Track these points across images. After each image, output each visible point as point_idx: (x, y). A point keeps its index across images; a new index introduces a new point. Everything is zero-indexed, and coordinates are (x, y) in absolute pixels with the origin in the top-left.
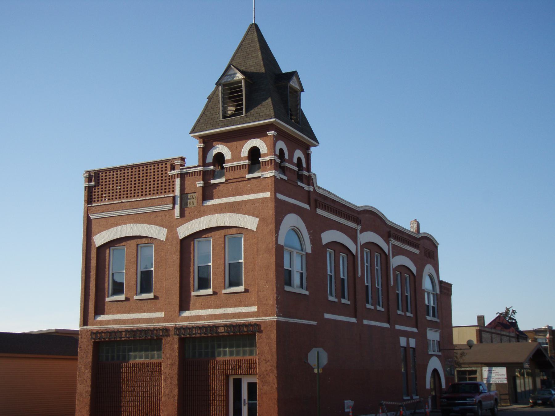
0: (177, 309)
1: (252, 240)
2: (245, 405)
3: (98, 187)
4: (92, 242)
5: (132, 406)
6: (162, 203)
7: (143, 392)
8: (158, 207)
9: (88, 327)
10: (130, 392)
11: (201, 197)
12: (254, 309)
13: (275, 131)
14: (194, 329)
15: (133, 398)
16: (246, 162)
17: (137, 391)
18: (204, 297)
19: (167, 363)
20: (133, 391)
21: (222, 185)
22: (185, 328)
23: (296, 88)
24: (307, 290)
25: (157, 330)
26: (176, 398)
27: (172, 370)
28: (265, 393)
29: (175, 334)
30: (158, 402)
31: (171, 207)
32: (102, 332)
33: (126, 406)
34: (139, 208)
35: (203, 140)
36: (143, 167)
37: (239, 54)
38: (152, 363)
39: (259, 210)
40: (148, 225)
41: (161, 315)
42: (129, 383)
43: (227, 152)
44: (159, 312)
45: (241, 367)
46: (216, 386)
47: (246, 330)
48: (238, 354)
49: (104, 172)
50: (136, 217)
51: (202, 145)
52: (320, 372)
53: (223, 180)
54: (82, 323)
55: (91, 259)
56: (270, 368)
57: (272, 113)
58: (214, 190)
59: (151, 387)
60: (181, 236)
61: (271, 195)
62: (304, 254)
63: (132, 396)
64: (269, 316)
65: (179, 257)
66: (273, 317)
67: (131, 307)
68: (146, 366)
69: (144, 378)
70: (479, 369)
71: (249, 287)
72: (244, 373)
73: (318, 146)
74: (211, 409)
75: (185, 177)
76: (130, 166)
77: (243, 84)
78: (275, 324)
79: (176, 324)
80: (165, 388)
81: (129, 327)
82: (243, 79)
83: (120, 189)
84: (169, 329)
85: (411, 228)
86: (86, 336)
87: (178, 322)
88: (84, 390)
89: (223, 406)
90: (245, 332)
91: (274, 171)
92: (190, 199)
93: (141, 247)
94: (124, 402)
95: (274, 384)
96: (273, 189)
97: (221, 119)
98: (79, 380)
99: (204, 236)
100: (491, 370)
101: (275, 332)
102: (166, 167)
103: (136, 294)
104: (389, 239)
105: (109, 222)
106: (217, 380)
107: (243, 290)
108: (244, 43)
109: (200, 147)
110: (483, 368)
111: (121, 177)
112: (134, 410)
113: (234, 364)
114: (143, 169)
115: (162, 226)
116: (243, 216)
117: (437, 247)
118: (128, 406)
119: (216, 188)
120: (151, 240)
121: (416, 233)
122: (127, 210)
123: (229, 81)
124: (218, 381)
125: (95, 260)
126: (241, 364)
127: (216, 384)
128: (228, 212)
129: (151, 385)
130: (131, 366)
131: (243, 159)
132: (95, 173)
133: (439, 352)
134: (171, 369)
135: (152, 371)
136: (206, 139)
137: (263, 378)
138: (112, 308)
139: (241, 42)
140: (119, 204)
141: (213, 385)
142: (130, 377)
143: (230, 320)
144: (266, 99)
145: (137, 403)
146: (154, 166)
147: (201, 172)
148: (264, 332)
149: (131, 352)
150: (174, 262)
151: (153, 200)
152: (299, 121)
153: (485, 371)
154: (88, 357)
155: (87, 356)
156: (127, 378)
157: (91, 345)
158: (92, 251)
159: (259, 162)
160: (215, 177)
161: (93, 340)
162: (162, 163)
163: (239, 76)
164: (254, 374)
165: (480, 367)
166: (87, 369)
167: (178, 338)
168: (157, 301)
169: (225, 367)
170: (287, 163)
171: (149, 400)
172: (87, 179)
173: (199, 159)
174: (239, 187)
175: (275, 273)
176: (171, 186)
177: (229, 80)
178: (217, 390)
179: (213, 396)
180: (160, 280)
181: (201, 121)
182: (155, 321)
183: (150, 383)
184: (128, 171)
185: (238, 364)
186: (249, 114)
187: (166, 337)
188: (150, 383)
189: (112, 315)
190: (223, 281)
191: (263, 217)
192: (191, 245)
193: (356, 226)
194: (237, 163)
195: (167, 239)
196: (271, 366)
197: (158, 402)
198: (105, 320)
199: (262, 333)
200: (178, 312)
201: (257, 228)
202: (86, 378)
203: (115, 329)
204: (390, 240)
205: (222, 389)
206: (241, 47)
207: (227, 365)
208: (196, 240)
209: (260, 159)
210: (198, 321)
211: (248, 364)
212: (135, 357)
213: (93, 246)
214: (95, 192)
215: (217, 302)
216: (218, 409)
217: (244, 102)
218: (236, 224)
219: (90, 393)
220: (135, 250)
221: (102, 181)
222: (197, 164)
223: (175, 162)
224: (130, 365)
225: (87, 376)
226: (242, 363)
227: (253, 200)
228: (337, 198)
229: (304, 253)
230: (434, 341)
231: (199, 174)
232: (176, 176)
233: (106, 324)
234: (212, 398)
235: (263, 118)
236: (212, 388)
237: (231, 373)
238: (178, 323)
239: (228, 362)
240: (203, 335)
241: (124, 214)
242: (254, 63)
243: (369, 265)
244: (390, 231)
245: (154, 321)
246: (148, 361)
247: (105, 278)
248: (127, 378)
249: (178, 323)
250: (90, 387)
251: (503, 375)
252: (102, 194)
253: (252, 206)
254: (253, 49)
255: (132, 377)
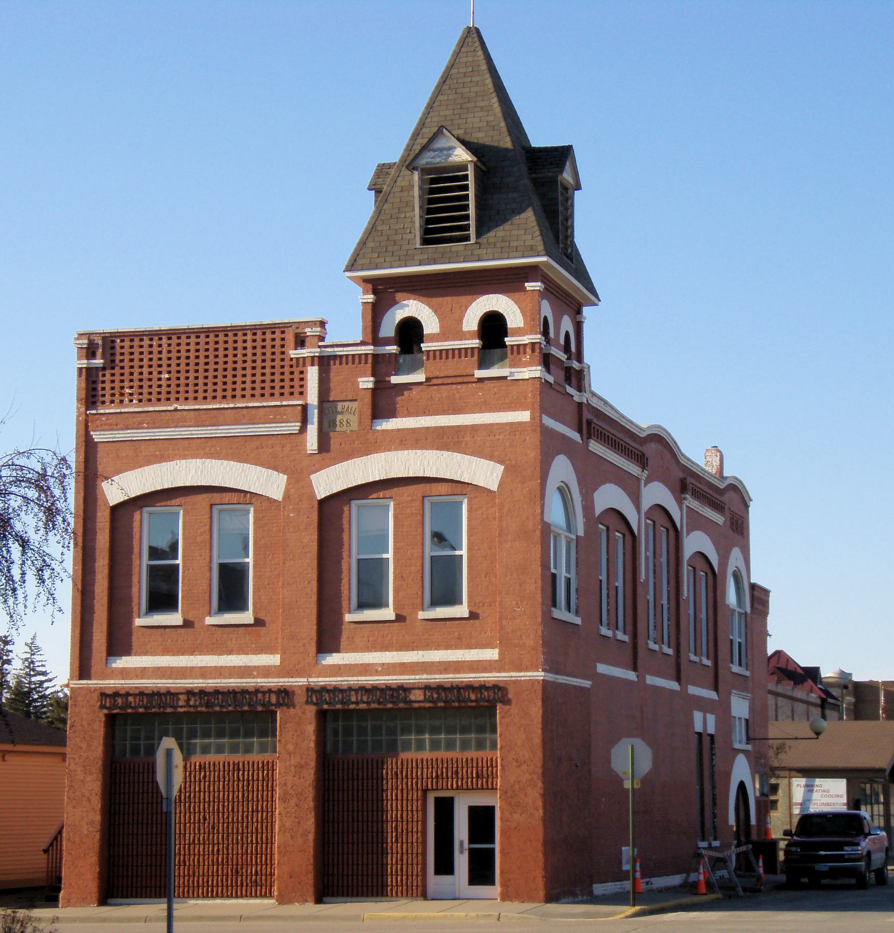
0: (313, 648)
1: (487, 510)
2: (462, 852)
3: (113, 372)
4: (98, 493)
5: (199, 855)
6: (275, 418)
7: (225, 825)
8: (266, 425)
9: (93, 683)
10: (195, 823)
11: (368, 412)
12: (492, 654)
13: (543, 282)
14: (353, 693)
15: (201, 837)
16: (476, 343)
17: (211, 821)
18: (375, 625)
19: (288, 763)
20: (202, 821)
21: (415, 391)
22: (330, 690)
23: (568, 182)
24: (577, 613)
25: (264, 693)
26: (311, 837)
27: (300, 778)
28: (515, 828)
29: (307, 703)
30: (264, 845)
31: (298, 428)
32: (128, 694)
33: (185, 855)
34: (219, 425)
35: (373, 286)
36: (226, 335)
37: (446, 97)
38: (248, 763)
39: (505, 449)
40: (239, 464)
41: (274, 660)
42: (192, 805)
43: (429, 318)
44: (266, 653)
45: (457, 772)
46: (399, 813)
47: (473, 697)
48: (450, 746)
49: (127, 339)
50: (209, 444)
51: (370, 298)
52: (635, 786)
53: (419, 377)
54: (77, 674)
55: (97, 532)
56: (527, 776)
57: (541, 247)
58: (399, 399)
59: (245, 814)
60: (321, 494)
61: (533, 418)
62: (572, 539)
63: (199, 833)
64: (527, 669)
65: (315, 537)
66: (535, 674)
67: (196, 640)
68: (234, 768)
69: (229, 794)
70: (783, 783)
71: (479, 608)
72: (465, 787)
73: (596, 305)
74: (389, 859)
75: (329, 365)
76: (194, 329)
77: (470, 173)
78: (539, 689)
79: (310, 680)
80: (284, 815)
81: (196, 685)
82: (471, 161)
83: (169, 379)
84: (293, 692)
85: (706, 465)
86: (88, 702)
87: (315, 677)
88: (83, 818)
89: (417, 853)
90: (472, 701)
91: (539, 368)
92: (342, 413)
93: (220, 511)
94: (180, 845)
95: (537, 810)
96: (537, 406)
97: (418, 246)
98: (69, 798)
99: (373, 496)
100: (812, 786)
101: (539, 703)
102: (283, 339)
103: (210, 614)
104: (683, 496)
105: (141, 452)
106: (402, 800)
107: (466, 615)
108: (454, 71)
109: (366, 301)
110: (794, 779)
111: (169, 352)
112: (204, 863)
113: (442, 768)
114: (226, 339)
115: (275, 468)
116: (467, 458)
117: (749, 506)
118: (189, 855)
119: (403, 395)
120: (245, 496)
121: (717, 476)
122: (187, 429)
123: (438, 163)
124: (405, 802)
125: (108, 534)
126: (457, 767)
127: (399, 807)
128: (432, 448)
129: (245, 809)
130: (197, 767)
131: (468, 336)
132: (104, 339)
133: (747, 744)
134: (297, 777)
135: (248, 780)
136: (380, 285)
137: (511, 797)
138: (149, 641)
139: (447, 67)
140: (168, 413)
141: (392, 811)
142: (195, 792)
143: (437, 676)
144: (520, 211)
145: (211, 849)
146: (254, 334)
147: (370, 356)
148: (514, 702)
149: (195, 737)
150: (303, 548)
151: (254, 411)
152: (570, 254)
153: (798, 785)
154: (93, 748)
155: (89, 746)
156: (187, 794)
157: (101, 721)
158: (99, 514)
159: (504, 345)
160: (399, 369)
161: (105, 711)
162: (273, 330)
163: (461, 155)
164: (492, 789)
165: (786, 777)
166: (91, 774)
167: (315, 712)
168: (262, 630)
169: (422, 774)
170: (553, 348)
171: (242, 840)
172: (85, 351)
173: (364, 328)
174: (457, 396)
175: (539, 582)
176: (296, 383)
177: (438, 160)
178: (402, 821)
179: (394, 834)
180: (269, 584)
181: (370, 244)
182: (258, 674)
183: (243, 805)
184: (188, 341)
185: (452, 768)
186: (483, 240)
187: (285, 708)
188: (243, 805)
189: (215, 657)
190: (420, 593)
191: (513, 462)
192: (342, 513)
193: (640, 473)
194: (453, 343)
195: (287, 496)
196: (530, 774)
197: (264, 845)
198: (135, 668)
199: (510, 705)
200: (315, 654)
201: (499, 485)
202: (87, 794)
203: (160, 688)
204: (685, 499)
205: (415, 819)
206: (448, 82)
207: (425, 770)
208: (354, 503)
209: (506, 339)
210: (361, 675)
211: (474, 769)
212: (205, 750)
213: (100, 502)
214: (103, 382)
215: (406, 637)
216: (405, 860)
217: (472, 211)
218: (451, 474)
219: (99, 827)
220: (208, 516)
221: (122, 358)
222: (359, 338)
223: (307, 330)
224: (195, 766)
225: (91, 788)
226: (460, 765)
227: (491, 425)
228: (616, 414)
229: (574, 537)
230: (740, 718)
231: (363, 361)
232: (308, 361)
233: (137, 677)
234: (390, 837)
235: (520, 254)
236: (392, 817)
237: (434, 787)
238: (315, 680)
239: (427, 763)
240: (373, 706)
241: (179, 437)
242: (485, 124)
243: (650, 554)
244: (685, 479)
245: (255, 673)
246: (238, 758)
247: (131, 575)
248: (187, 794)
249: (315, 680)
250: (98, 812)
251: (838, 796)
252: (122, 388)
253: (489, 438)
254: (477, 89)
255: (200, 791)
